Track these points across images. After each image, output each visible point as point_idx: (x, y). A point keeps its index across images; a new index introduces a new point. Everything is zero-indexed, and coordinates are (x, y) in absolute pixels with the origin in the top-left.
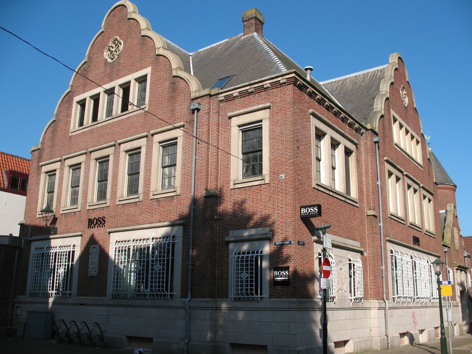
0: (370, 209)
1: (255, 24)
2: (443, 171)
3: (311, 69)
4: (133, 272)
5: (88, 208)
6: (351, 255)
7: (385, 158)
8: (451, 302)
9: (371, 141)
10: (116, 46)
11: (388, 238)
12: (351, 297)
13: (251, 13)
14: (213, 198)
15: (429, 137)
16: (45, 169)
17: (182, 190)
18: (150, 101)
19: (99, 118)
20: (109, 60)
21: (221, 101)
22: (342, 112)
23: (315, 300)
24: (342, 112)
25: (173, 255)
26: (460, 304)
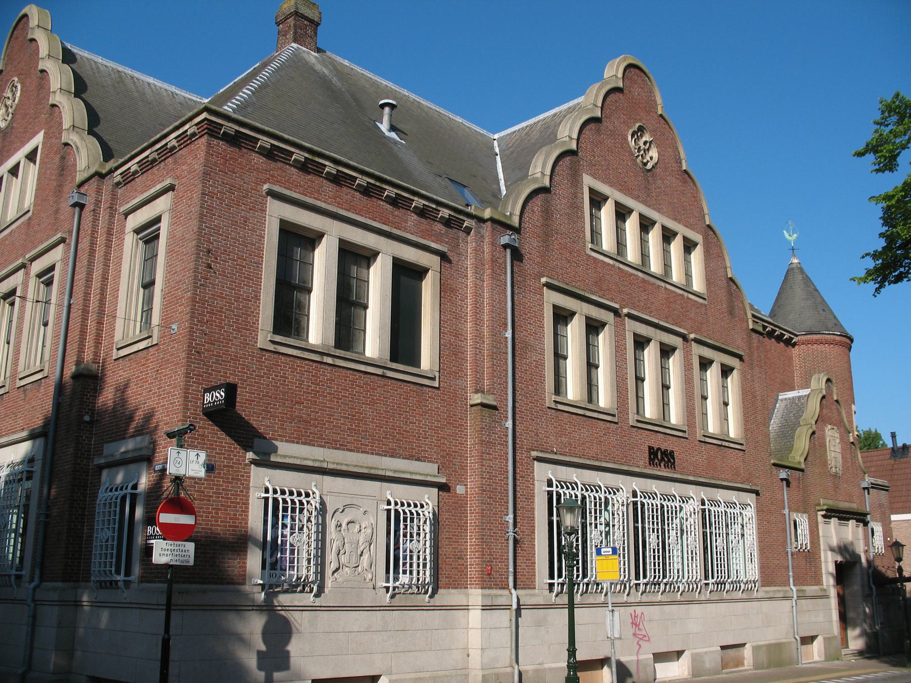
0: (477, 391)
1: (295, 25)
2: (821, 306)
3: (392, 107)
4: (11, 531)
7: (544, 280)
8: (794, 589)
9: (493, 244)
11: (534, 454)
12: (388, 580)
13: (288, 6)
14: (87, 380)
15: (795, 235)
21: (118, 184)
22: (384, 186)
23: (247, 588)
24: (384, 186)
26: (833, 592)
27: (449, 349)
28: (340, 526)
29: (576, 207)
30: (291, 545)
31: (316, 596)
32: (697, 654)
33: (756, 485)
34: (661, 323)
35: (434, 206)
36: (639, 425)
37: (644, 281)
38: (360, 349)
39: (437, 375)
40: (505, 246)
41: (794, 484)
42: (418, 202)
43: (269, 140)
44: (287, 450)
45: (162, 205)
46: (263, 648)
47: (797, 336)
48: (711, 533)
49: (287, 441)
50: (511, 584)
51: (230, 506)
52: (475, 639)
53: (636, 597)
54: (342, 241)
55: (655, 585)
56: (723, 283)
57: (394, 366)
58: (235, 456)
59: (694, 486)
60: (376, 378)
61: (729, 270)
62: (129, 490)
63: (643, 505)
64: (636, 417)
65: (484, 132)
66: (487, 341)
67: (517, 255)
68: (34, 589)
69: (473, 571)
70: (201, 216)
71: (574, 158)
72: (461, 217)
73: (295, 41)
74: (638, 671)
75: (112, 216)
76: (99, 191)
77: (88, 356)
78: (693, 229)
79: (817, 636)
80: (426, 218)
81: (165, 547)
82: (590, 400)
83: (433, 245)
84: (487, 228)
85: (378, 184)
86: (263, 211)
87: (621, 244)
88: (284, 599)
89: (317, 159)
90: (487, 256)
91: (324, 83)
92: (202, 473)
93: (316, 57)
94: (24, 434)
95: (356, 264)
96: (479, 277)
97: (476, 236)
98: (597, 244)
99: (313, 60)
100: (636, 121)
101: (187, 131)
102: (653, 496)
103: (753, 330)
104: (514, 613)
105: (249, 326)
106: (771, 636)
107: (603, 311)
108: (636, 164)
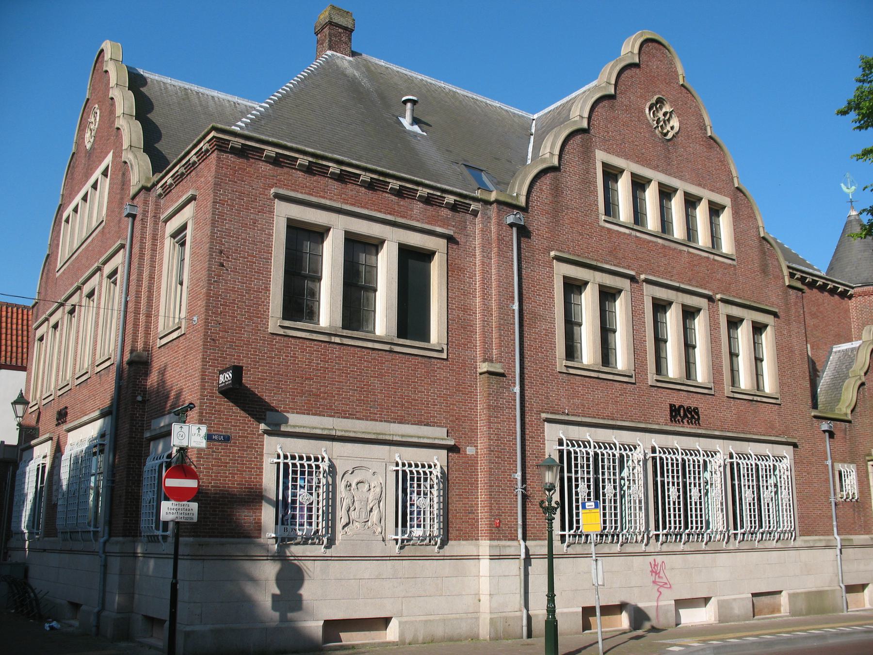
0: (485, 361)
1: (330, 34)
3: (414, 102)
7: (553, 254)
9: (499, 224)
11: (544, 415)
12: (397, 534)
13: (323, 16)
15: (853, 188)
21: (160, 195)
27: (457, 324)
28: (350, 485)
29: (588, 182)
30: (301, 503)
31: (326, 547)
32: (724, 601)
33: (793, 437)
34: (682, 286)
35: (439, 194)
36: (659, 384)
37: (664, 246)
38: (370, 328)
39: (445, 347)
40: (511, 225)
41: (838, 435)
42: (423, 191)
43: (273, 149)
44: (297, 421)
45: (188, 212)
46: (277, 591)
47: (853, 288)
49: (297, 413)
50: (520, 536)
51: (245, 471)
52: (485, 586)
53: (655, 546)
54: (753, 322)
55: (752, 534)
56: (755, 243)
57: (401, 341)
58: (249, 427)
59: (722, 441)
60: (384, 353)
61: (761, 229)
62: (165, 459)
64: (656, 377)
65: (524, 114)
66: (495, 314)
67: (523, 232)
68: (105, 543)
69: (483, 524)
70: (213, 223)
71: (586, 136)
72: (467, 201)
73: (330, 48)
74: (657, 616)
75: (156, 223)
76: (146, 203)
77: (140, 346)
78: (720, 193)
79: (868, 584)
80: (432, 205)
81: (170, 506)
83: (439, 229)
84: (493, 210)
85: (381, 178)
86: (272, 212)
87: (639, 215)
88: (295, 550)
89: (320, 162)
90: (494, 236)
91: (353, 86)
92: (203, 444)
93: (350, 62)
94: (97, 413)
95: (365, 252)
96: (486, 255)
97: (483, 217)
98: (614, 217)
99: (346, 64)
101: (202, 148)
102: (674, 451)
103: (790, 287)
104: (523, 562)
105: (259, 313)
106: (812, 584)
107: (618, 279)
108: (655, 135)
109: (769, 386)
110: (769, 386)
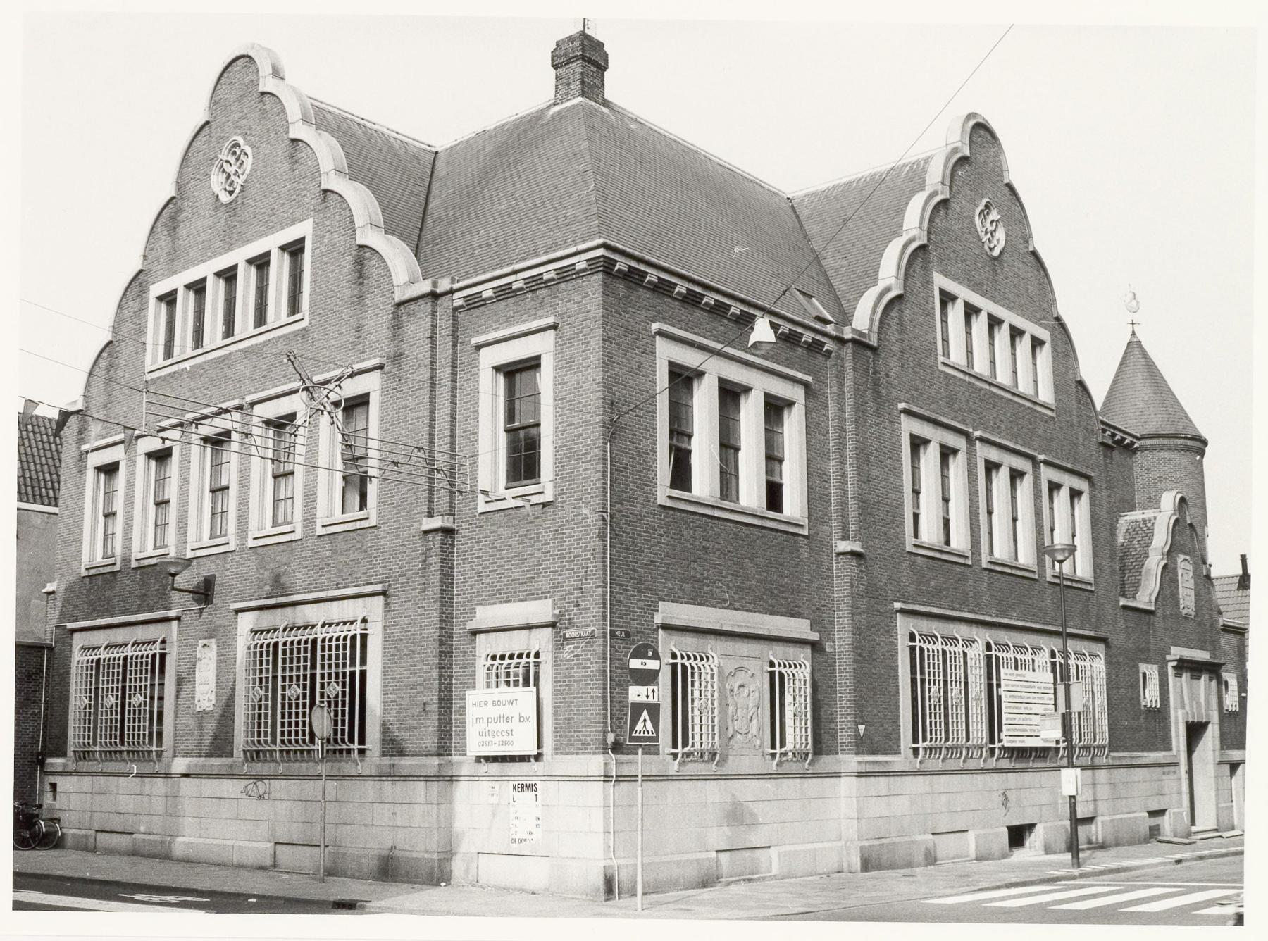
5: (251, 543)
6: (776, 653)
10: (237, 159)
11: (897, 605)
16: (96, 459)
17: (380, 516)
18: (313, 303)
19: (176, 350)
20: (225, 198)
25: (364, 662)
27: (816, 497)
48: (923, 681)
54: (767, 395)
63: (922, 650)
64: (913, 541)
82: (948, 542)
100: (983, 197)
105: (648, 483)
109: (541, 610)
110: (541, 610)
